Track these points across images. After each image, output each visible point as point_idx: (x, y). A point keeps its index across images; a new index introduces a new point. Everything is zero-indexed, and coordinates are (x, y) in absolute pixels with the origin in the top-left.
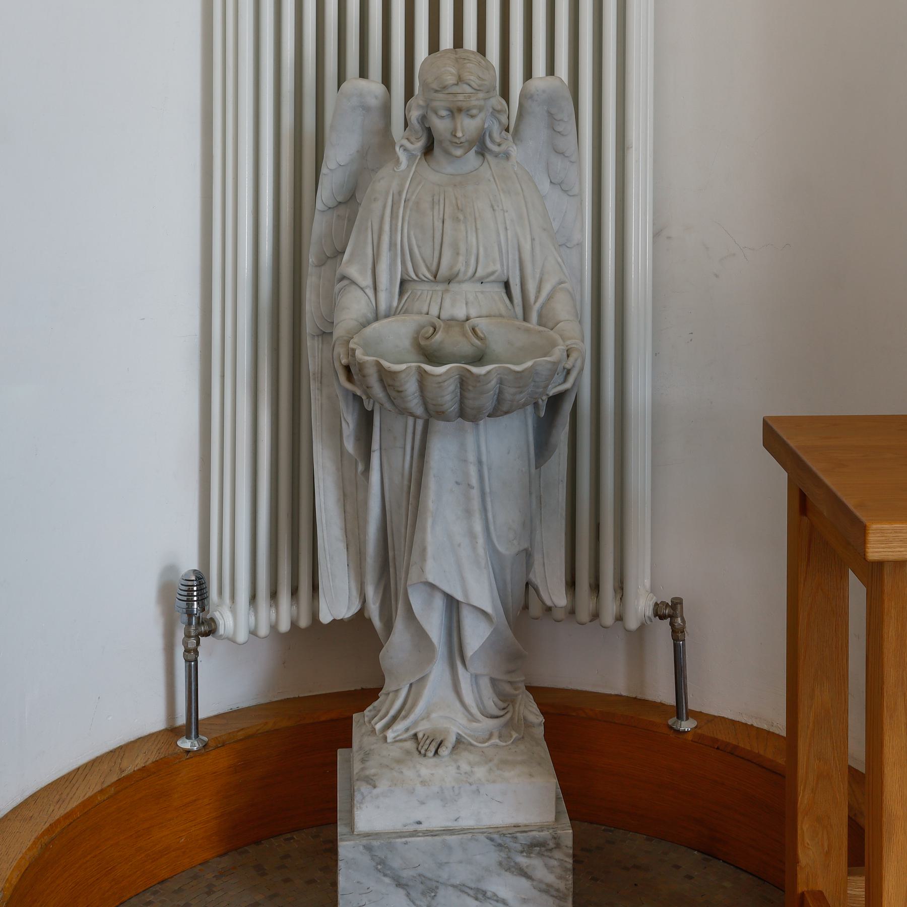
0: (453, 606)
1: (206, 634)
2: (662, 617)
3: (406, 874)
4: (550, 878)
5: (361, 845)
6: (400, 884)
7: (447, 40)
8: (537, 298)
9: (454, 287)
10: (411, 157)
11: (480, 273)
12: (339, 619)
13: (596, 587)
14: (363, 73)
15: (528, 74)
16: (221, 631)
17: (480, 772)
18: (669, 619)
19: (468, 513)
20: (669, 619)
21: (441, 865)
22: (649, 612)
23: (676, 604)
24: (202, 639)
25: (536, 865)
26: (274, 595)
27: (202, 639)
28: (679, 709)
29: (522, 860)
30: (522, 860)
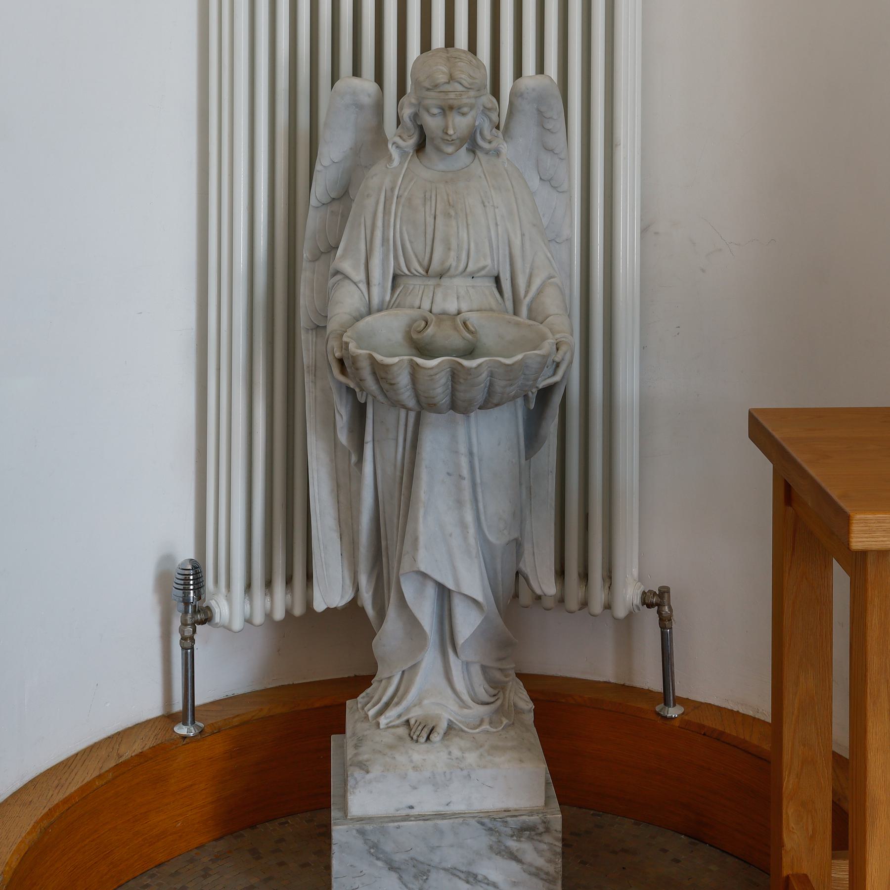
0: (444, 594)
1: (202, 622)
2: (650, 606)
3: (398, 858)
4: (540, 862)
5: (354, 829)
6: (392, 867)
7: (438, 39)
8: (527, 292)
9: (445, 281)
10: (403, 154)
11: (471, 268)
12: (333, 607)
13: (585, 576)
14: (357, 71)
15: (518, 72)
16: (217, 619)
17: (471, 758)
18: (657, 607)
19: (459, 503)
20: (657, 607)
21: (432, 849)
22: (637, 601)
23: (664, 592)
24: (198, 627)
25: (526, 849)
26: (269, 584)
27: (198, 627)
28: (667, 696)
29: (512, 844)
30: (512, 844)
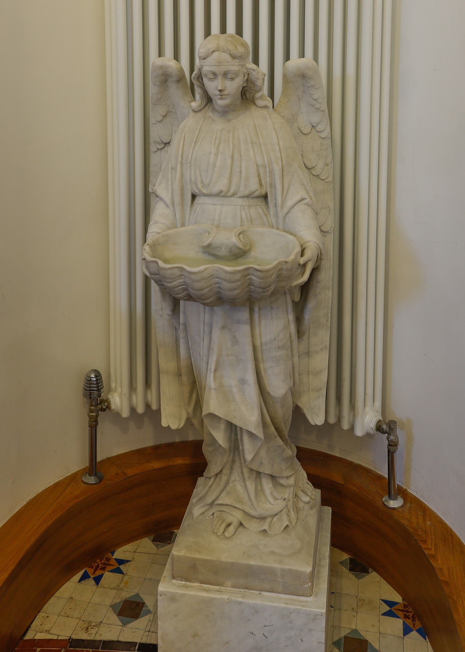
1: (103, 410)
2: (383, 432)
14: (223, 30)
16: (113, 407)
22: (373, 425)
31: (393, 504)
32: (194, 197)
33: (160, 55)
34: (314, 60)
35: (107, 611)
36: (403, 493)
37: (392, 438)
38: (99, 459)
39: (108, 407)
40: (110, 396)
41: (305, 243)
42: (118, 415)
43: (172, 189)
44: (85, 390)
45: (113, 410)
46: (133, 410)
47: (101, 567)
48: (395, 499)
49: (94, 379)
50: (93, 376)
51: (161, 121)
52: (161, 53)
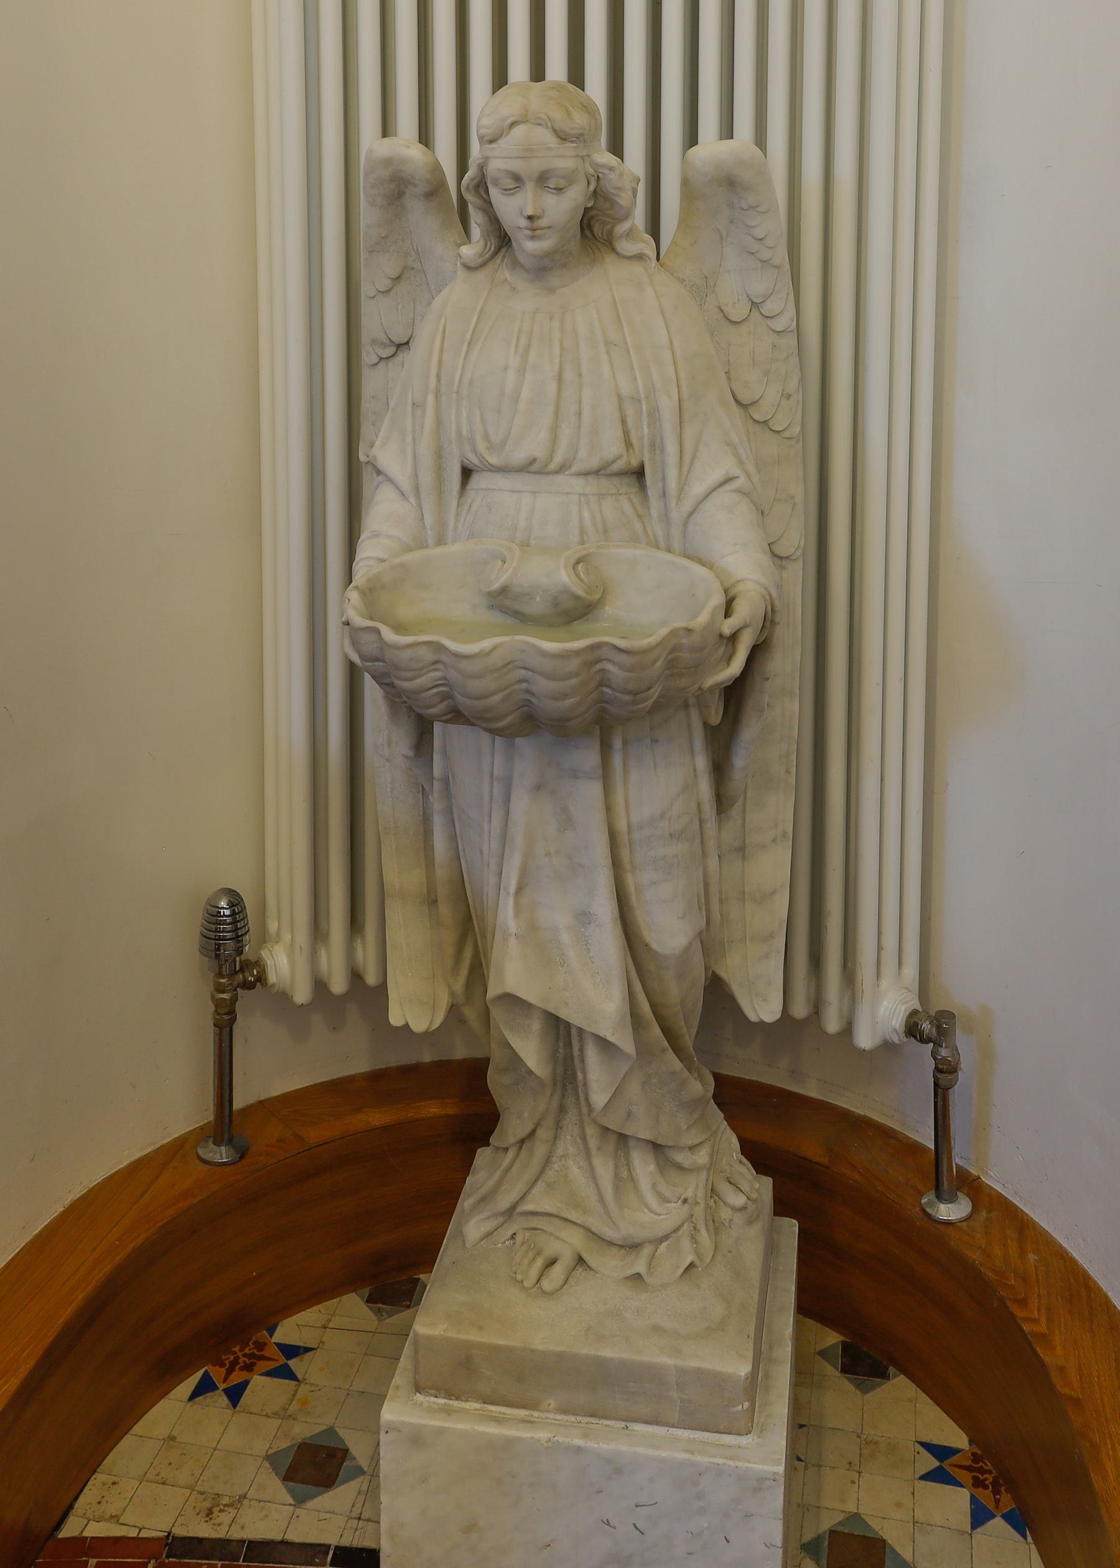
1: (248, 986)
2: (923, 1040)
14: (538, 72)
16: (272, 978)
22: (898, 1022)
31: (947, 1212)
32: (467, 473)
33: (385, 133)
34: (756, 145)
35: (258, 1470)
36: (970, 1185)
37: (944, 1052)
38: (238, 1104)
39: (261, 979)
40: (264, 953)
41: (734, 585)
42: (283, 997)
43: (415, 456)
44: (204, 938)
45: (273, 985)
46: (320, 986)
47: (242, 1364)
48: (952, 1199)
49: (227, 912)
50: (223, 904)
51: (388, 291)
52: (387, 129)
